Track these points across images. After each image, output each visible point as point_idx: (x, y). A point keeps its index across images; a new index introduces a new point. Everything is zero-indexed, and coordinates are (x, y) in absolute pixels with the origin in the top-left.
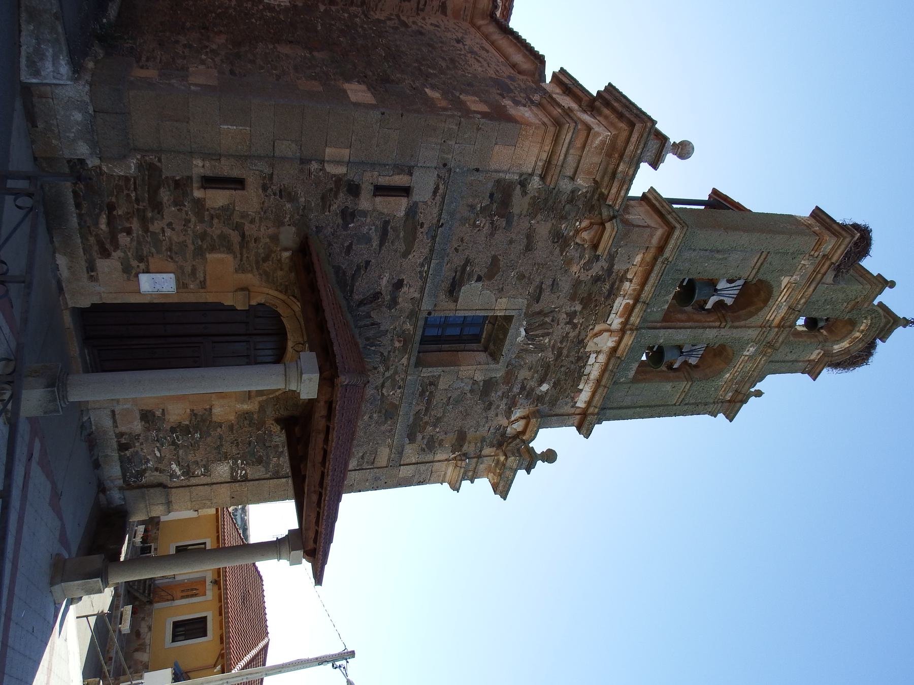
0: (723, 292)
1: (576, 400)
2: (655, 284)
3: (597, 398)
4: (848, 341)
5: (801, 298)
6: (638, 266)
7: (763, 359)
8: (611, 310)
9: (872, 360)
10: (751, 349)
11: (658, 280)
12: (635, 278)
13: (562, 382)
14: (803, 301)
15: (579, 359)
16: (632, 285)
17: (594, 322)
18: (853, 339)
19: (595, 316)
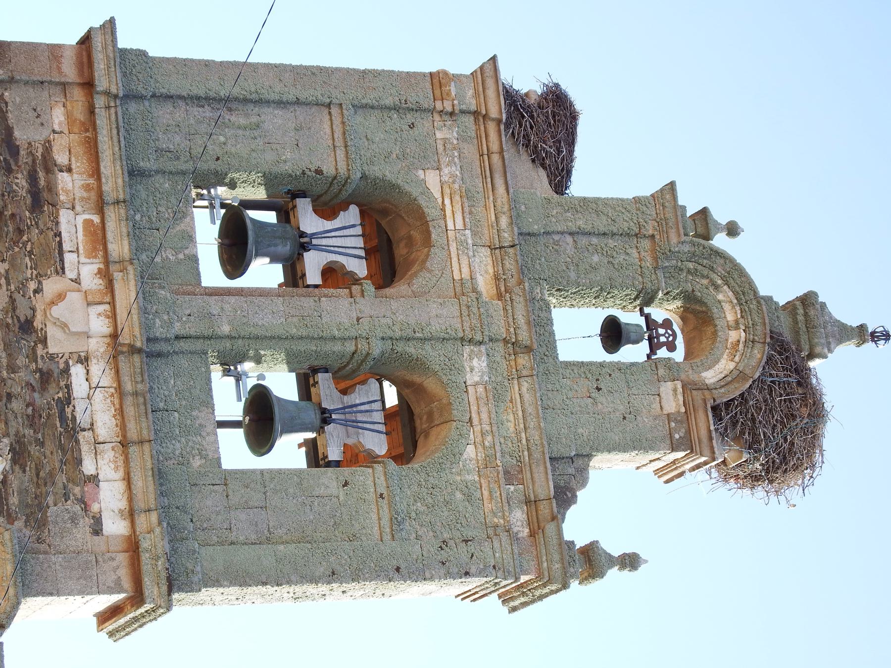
0: (324, 242)
1: (95, 507)
2: (117, 156)
3: (138, 483)
4: (725, 356)
5: (496, 218)
6: (66, 131)
7: (524, 389)
8: (60, 244)
9: (578, 106)
10: (475, 362)
11: (116, 144)
12: (73, 159)
13: (33, 449)
14: (504, 221)
15: (46, 378)
16: (75, 176)
17: (35, 272)
18: (733, 347)
19: (31, 259)
